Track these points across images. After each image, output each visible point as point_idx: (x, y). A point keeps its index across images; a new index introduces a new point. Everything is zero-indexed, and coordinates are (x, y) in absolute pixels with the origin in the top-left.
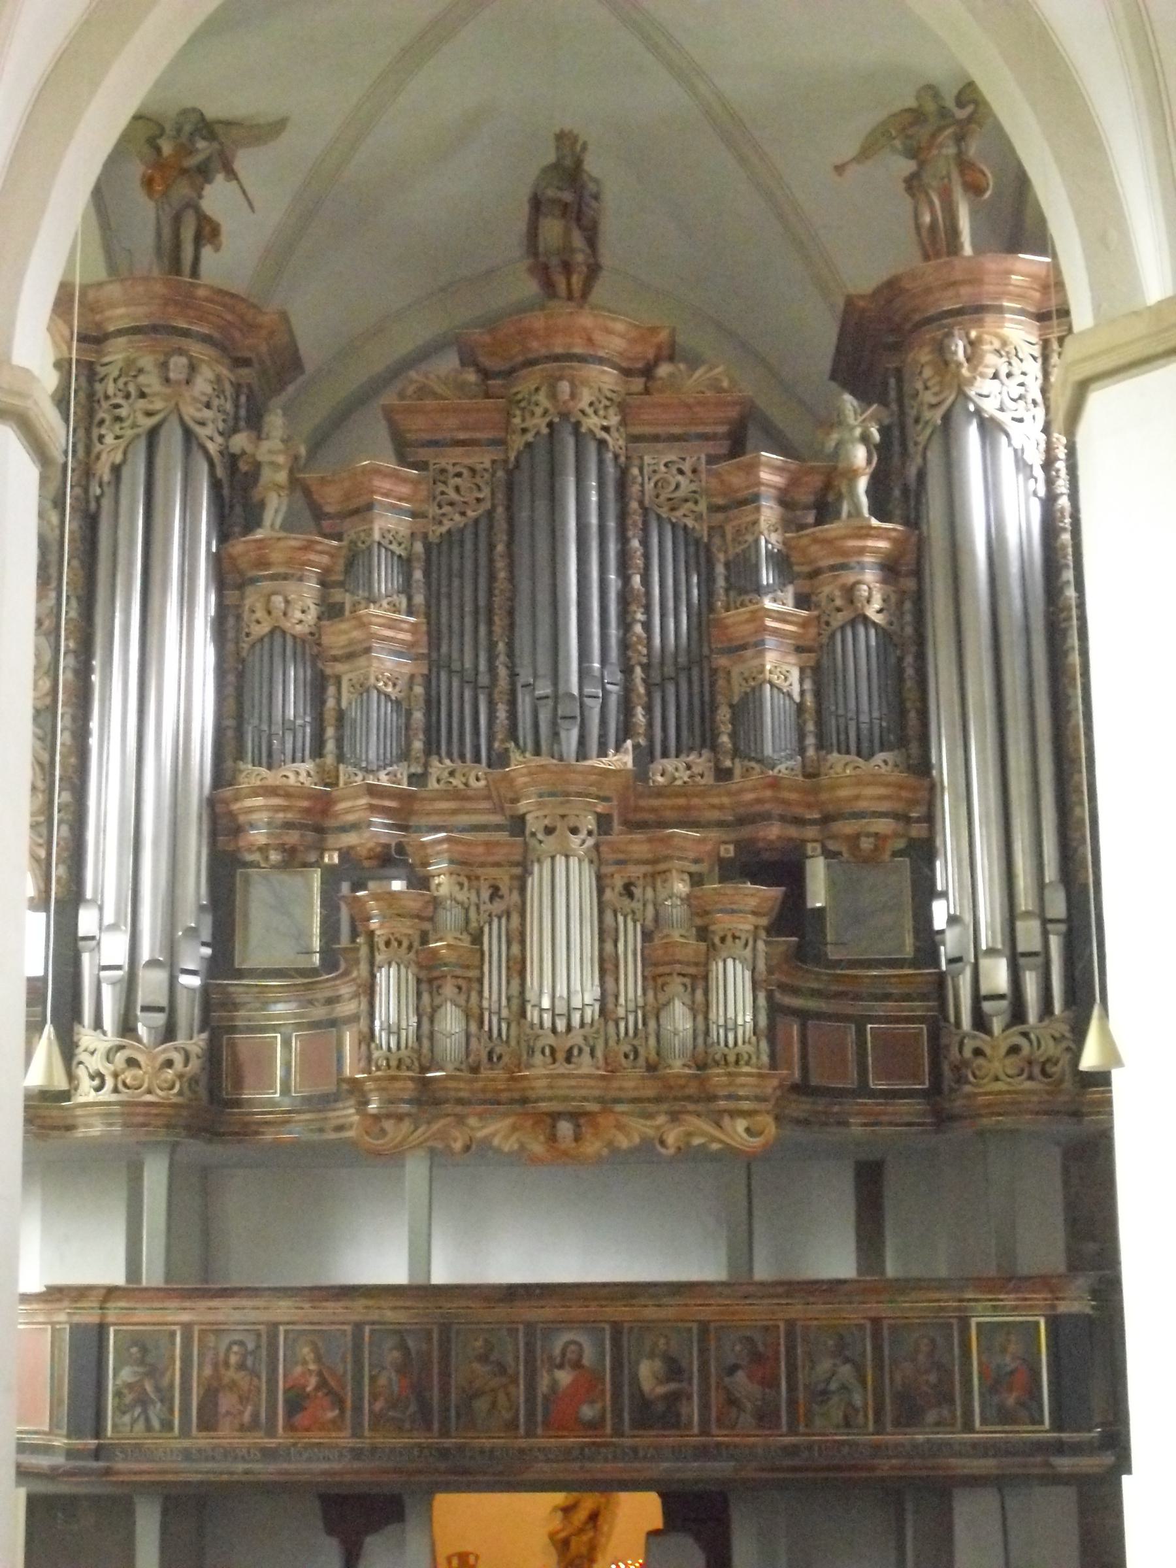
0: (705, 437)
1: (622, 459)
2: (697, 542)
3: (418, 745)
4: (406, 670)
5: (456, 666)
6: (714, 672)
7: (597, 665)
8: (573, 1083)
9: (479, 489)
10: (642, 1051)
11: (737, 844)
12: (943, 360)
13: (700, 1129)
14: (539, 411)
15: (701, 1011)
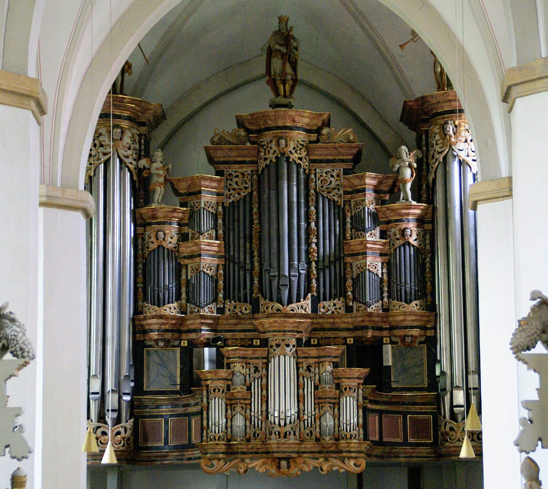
0: (342, 161)
1: (307, 171)
2: (339, 207)
3: (221, 295)
4: (216, 263)
5: (236, 260)
6: (345, 264)
7: (296, 263)
8: (287, 446)
9: (246, 183)
10: (313, 432)
11: (354, 338)
12: (444, 133)
13: (336, 464)
14: (272, 151)
15: (337, 417)
